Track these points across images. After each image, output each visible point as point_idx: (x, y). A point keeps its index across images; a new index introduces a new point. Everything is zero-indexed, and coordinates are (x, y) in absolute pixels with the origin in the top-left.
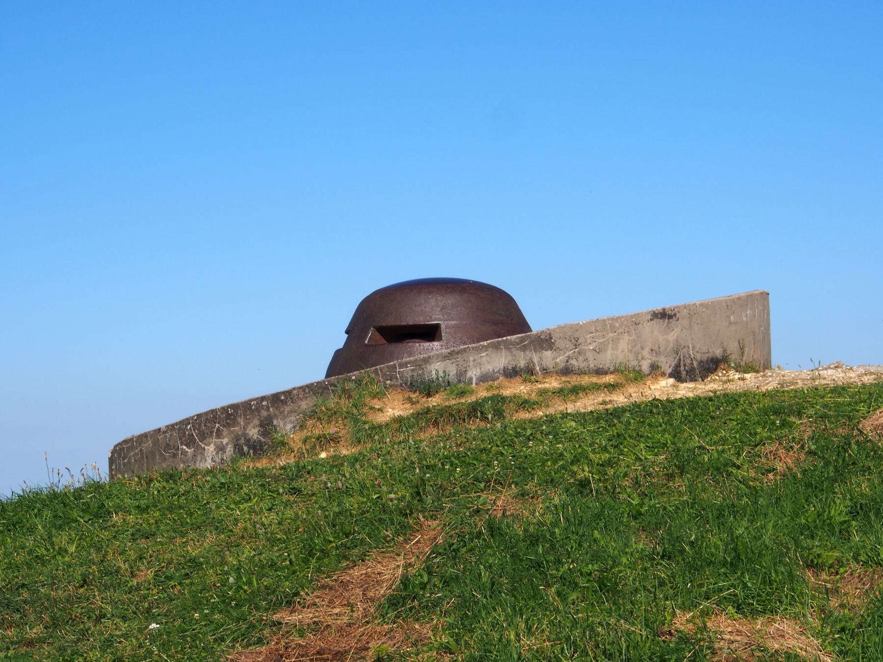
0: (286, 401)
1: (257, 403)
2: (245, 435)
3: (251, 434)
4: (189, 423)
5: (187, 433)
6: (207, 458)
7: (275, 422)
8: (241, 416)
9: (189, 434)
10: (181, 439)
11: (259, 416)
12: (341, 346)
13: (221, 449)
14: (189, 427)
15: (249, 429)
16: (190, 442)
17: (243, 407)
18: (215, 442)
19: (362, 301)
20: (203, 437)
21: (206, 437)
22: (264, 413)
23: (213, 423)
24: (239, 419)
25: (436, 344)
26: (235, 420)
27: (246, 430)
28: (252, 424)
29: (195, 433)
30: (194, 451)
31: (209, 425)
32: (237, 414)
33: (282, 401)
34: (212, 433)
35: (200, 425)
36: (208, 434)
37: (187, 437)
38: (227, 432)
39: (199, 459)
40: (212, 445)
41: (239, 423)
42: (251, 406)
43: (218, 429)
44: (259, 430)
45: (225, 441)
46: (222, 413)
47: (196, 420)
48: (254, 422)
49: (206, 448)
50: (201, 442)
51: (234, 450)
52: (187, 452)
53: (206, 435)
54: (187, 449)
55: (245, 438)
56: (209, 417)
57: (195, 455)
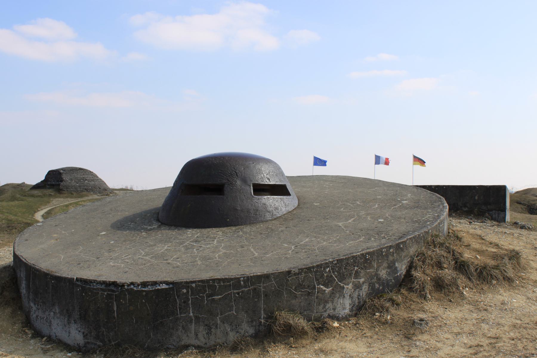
0: (403, 249)
1: (387, 251)
2: (377, 275)
3: (381, 274)
4: (329, 267)
5: (325, 275)
6: (346, 295)
7: (397, 265)
8: (375, 260)
9: (327, 276)
10: (318, 280)
11: (387, 260)
12: (135, 189)
13: (358, 287)
14: (328, 270)
15: (380, 270)
16: (328, 282)
17: (377, 253)
18: (354, 282)
19: (188, 163)
20: (342, 278)
21: (345, 278)
22: (391, 258)
23: (352, 266)
24: (373, 263)
25: (291, 196)
26: (370, 263)
27: (378, 272)
28: (382, 267)
29: (335, 275)
30: (333, 289)
31: (349, 268)
32: (372, 259)
33: (401, 248)
34: (350, 274)
35: (340, 268)
36: (347, 275)
37: (325, 278)
38: (364, 274)
39: (338, 295)
40: (351, 284)
41: (373, 267)
42: (382, 252)
43: (356, 272)
44: (387, 271)
45: (362, 280)
46: (361, 259)
47: (336, 264)
48: (384, 265)
49: (345, 286)
50: (340, 282)
51: (369, 288)
52: (325, 291)
53: (345, 276)
54: (324, 288)
55: (377, 277)
56: (349, 262)
57: (333, 293)
